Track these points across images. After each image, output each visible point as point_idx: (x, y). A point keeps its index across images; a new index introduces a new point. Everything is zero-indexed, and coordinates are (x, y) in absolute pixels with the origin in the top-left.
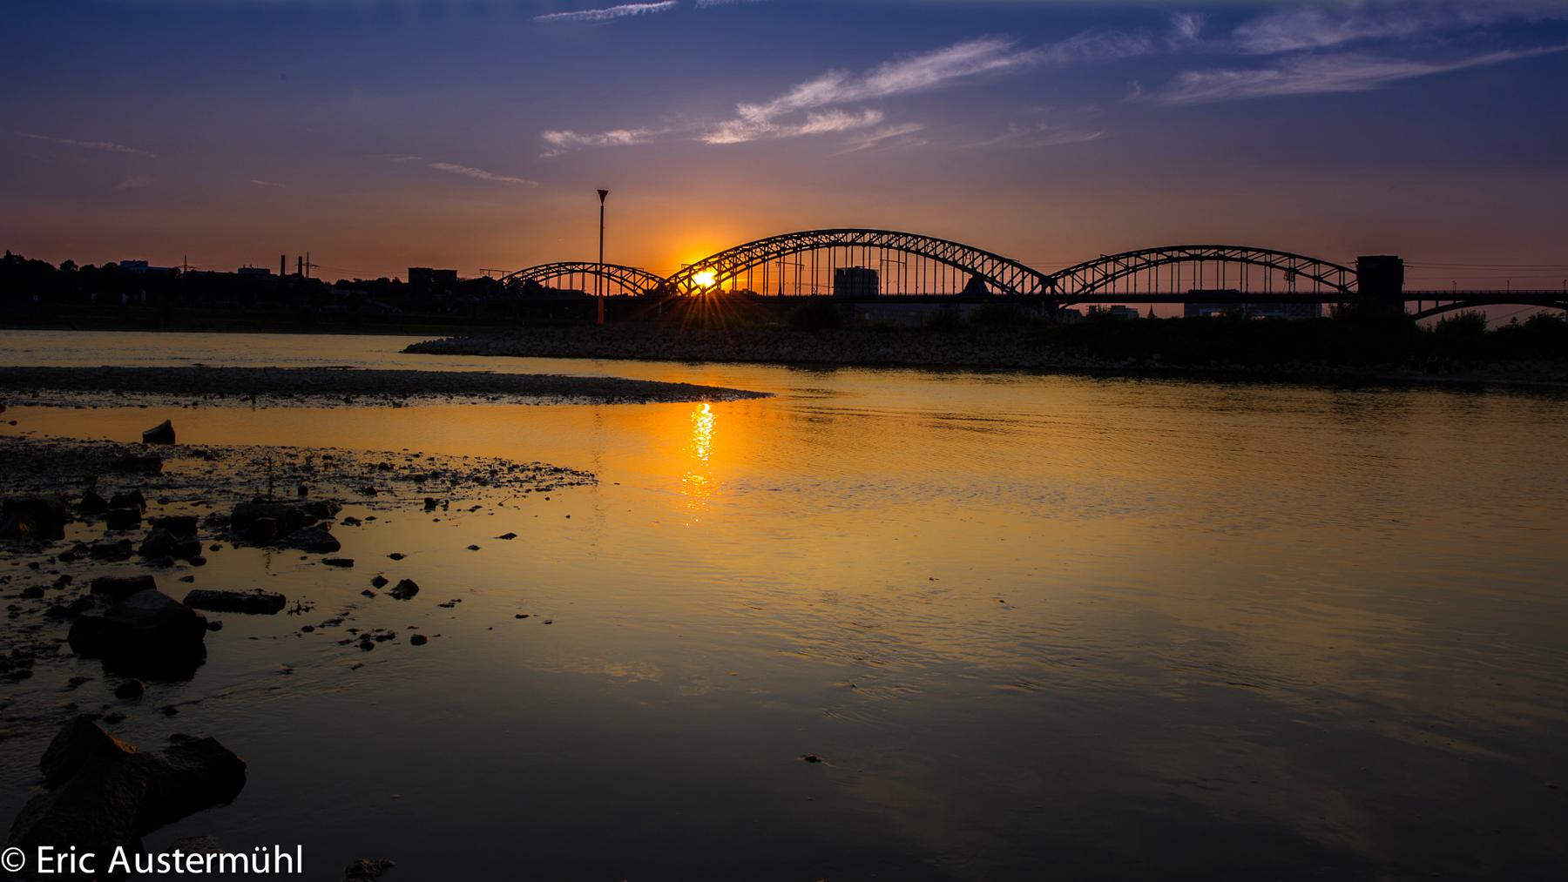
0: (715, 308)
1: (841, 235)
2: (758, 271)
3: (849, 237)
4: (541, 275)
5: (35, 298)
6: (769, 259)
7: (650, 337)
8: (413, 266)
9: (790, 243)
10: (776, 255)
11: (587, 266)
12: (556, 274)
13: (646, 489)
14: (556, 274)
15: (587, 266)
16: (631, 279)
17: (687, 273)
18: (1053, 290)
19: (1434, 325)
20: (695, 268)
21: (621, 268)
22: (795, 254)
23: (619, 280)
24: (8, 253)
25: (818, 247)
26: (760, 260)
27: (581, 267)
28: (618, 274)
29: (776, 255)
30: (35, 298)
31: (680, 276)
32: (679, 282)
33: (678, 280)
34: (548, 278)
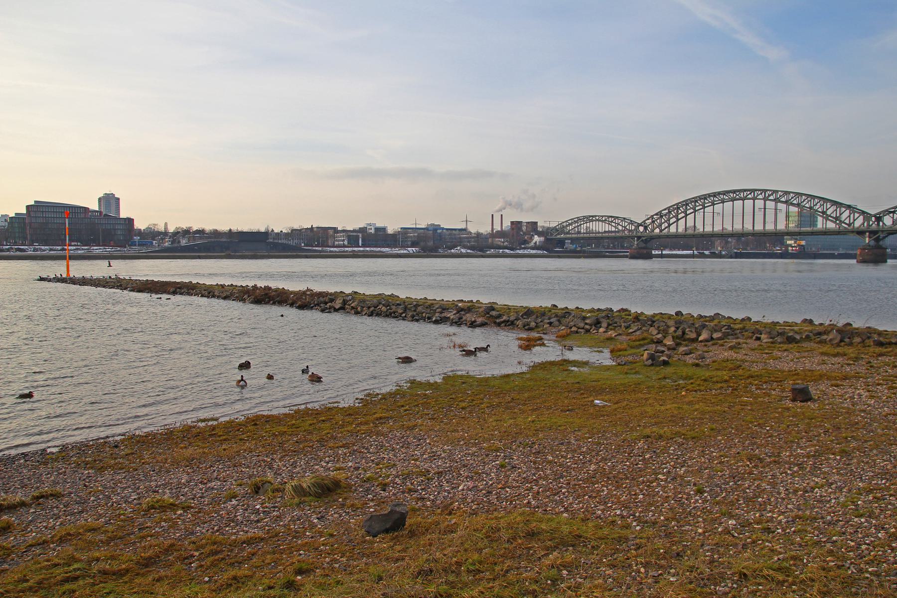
20: (655, 217)
26: (701, 207)
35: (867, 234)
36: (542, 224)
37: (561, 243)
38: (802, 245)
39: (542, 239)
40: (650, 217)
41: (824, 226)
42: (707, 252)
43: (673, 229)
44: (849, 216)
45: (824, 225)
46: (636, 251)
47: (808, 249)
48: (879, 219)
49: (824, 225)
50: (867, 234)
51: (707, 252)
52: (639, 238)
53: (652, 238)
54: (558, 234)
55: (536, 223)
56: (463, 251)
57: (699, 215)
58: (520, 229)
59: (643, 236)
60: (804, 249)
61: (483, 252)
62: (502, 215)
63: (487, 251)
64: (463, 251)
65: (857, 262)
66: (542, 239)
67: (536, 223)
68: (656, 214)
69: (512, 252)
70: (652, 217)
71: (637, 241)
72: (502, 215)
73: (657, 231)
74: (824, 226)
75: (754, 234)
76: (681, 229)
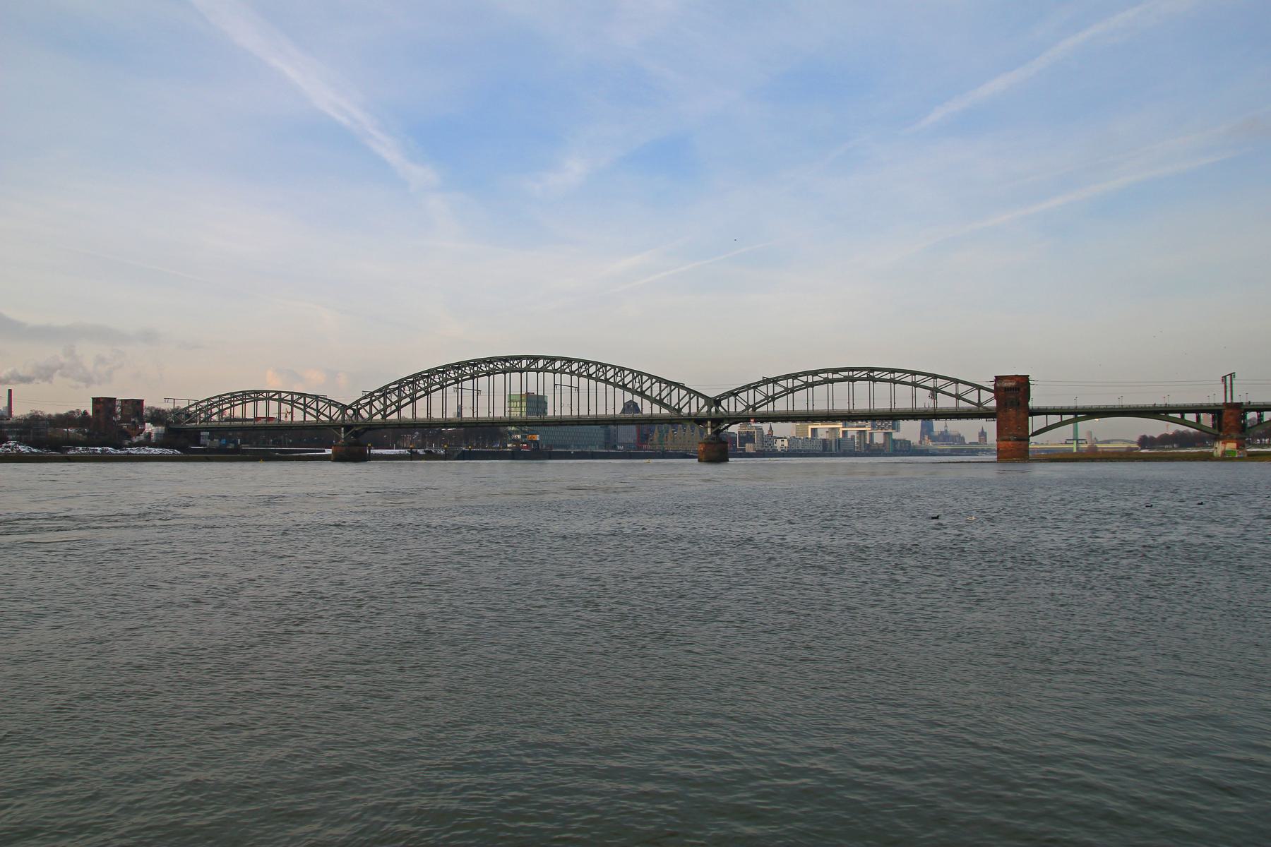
11: (271, 394)
15: (271, 394)
16: (314, 406)
17: (368, 400)
18: (717, 411)
20: (376, 394)
23: (302, 407)
26: (438, 386)
28: (302, 401)
31: (361, 402)
34: (234, 406)
35: (709, 423)
36: (154, 401)
37: (195, 435)
38: (536, 441)
39: (161, 429)
40: (368, 395)
41: (475, 416)
42: (421, 451)
43: (407, 413)
44: (679, 400)
45: (475, 414)
46: (344, 449)
47: (542, 446)
48: (717, 402)
49: (475, 414)
50: (709, 423)
51: (421, 451)
52: (348, 428)
53: (370, 427)
54: (189, 422)
55: (140, 402)
56: (24, 449)
57: (436, 396)
58: (112, 411)
59: (357, 426)
60: (538, 445)
61: (62, 453)
62: (10, 391)
63: (68, 449)
64: (24, 449)
65: (699, 461)
66: (161, 429)
67: (140, 402)
68: (380, 390)
69: (119, 451)
70: (372, 394)
71: (345, 433)
72: (10, 391)
73: (379, 417)
74: (475, 416)
75: (460, 424)
76: (422, 415)
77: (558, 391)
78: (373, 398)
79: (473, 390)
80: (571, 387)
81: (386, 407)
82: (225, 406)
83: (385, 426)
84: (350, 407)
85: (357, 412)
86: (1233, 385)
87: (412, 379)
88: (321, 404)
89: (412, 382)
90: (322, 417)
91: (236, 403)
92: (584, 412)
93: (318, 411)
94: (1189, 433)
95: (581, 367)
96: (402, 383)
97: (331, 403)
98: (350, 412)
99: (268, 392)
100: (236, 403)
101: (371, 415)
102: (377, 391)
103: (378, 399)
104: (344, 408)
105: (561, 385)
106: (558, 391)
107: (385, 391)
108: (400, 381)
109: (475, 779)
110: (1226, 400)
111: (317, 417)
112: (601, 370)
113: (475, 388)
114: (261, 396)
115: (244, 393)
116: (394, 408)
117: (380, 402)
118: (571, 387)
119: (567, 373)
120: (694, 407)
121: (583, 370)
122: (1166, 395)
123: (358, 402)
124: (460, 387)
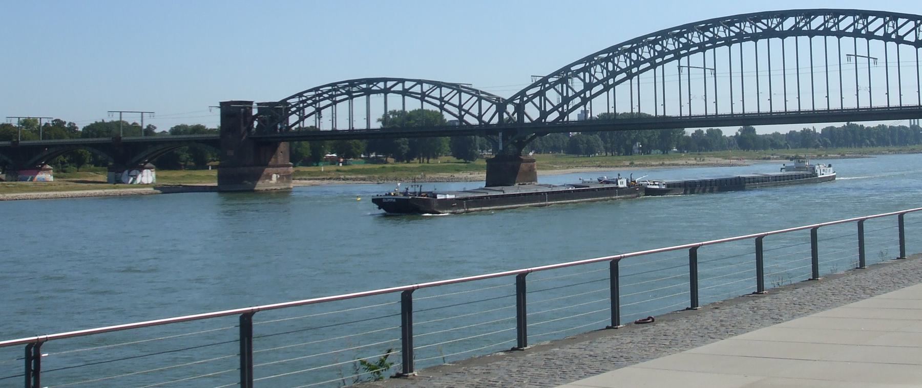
0: (855, 143)
1: (775, 21)
2: (623, 89)
3: (789, 23)
4: (325, 99)
5: (46, 149)
6: (592, 97)
7: (375, 374)
8: (221, 101)
9: (670, 45)
10: (672, 55)
11: (389, 84)
12: (346, 96)
13: (487, 386)
14: (346, 96)
15: (389, 84)
16: (455, 101)
17: (537, 89)
19: (819, 131)
20: (550, 80)
21: (439, 85)
22: (701, 54)
23: (438, 103)
24: (103, 120)
25: (714, 46)
26: (648, 65)
27: (381, 85)
28: (436, 93)
29: (672, 55)
30: (46, 149)
31: (528, 93)
32: (527, 102)
33: (525, 99)
34: (335, 103)
68: (557, 73)
70: (544, 80)
77: (684, 77)
78: (547, 85)
79: (689, 67)
80: (869, 58)
81: (566, 100)
82: (323, 104)
83: (562, 126)
84: (511, 100)
85: (520, 109)
86: (729, 72)
87: (605, 55)
88: (465, 97)
89: (607, 60)
90: (468, 118)
91: (338, 98)
92: (804, 108)
93: (460, 107)
94: (459, 209)
95: (828, 21)
96: (590, 61)
97: (478, 95)
98: (510, 108)
99: (385, 80)
100: (338, 98)
101: (544, 114)
102: (552, 76)
103: (553, 86)
104: (501, 105)
105: (856, 56)
106: (684, 77)
107: (564, 75)
108: (589, 59)
109: (110, 377)
110: (350, 128)
111: (461, 117)
112: (861, 21)
113: (685, 70)
114: (375, 88)
115: (352, 83)
116: (578, 100)
117: (573, 90)
118: (869, 58)
119: (878, 38)
120: (490, 115)
121: (830, 24)
122: (152, 117)
123: (522, 93)
124: (709, 64)
